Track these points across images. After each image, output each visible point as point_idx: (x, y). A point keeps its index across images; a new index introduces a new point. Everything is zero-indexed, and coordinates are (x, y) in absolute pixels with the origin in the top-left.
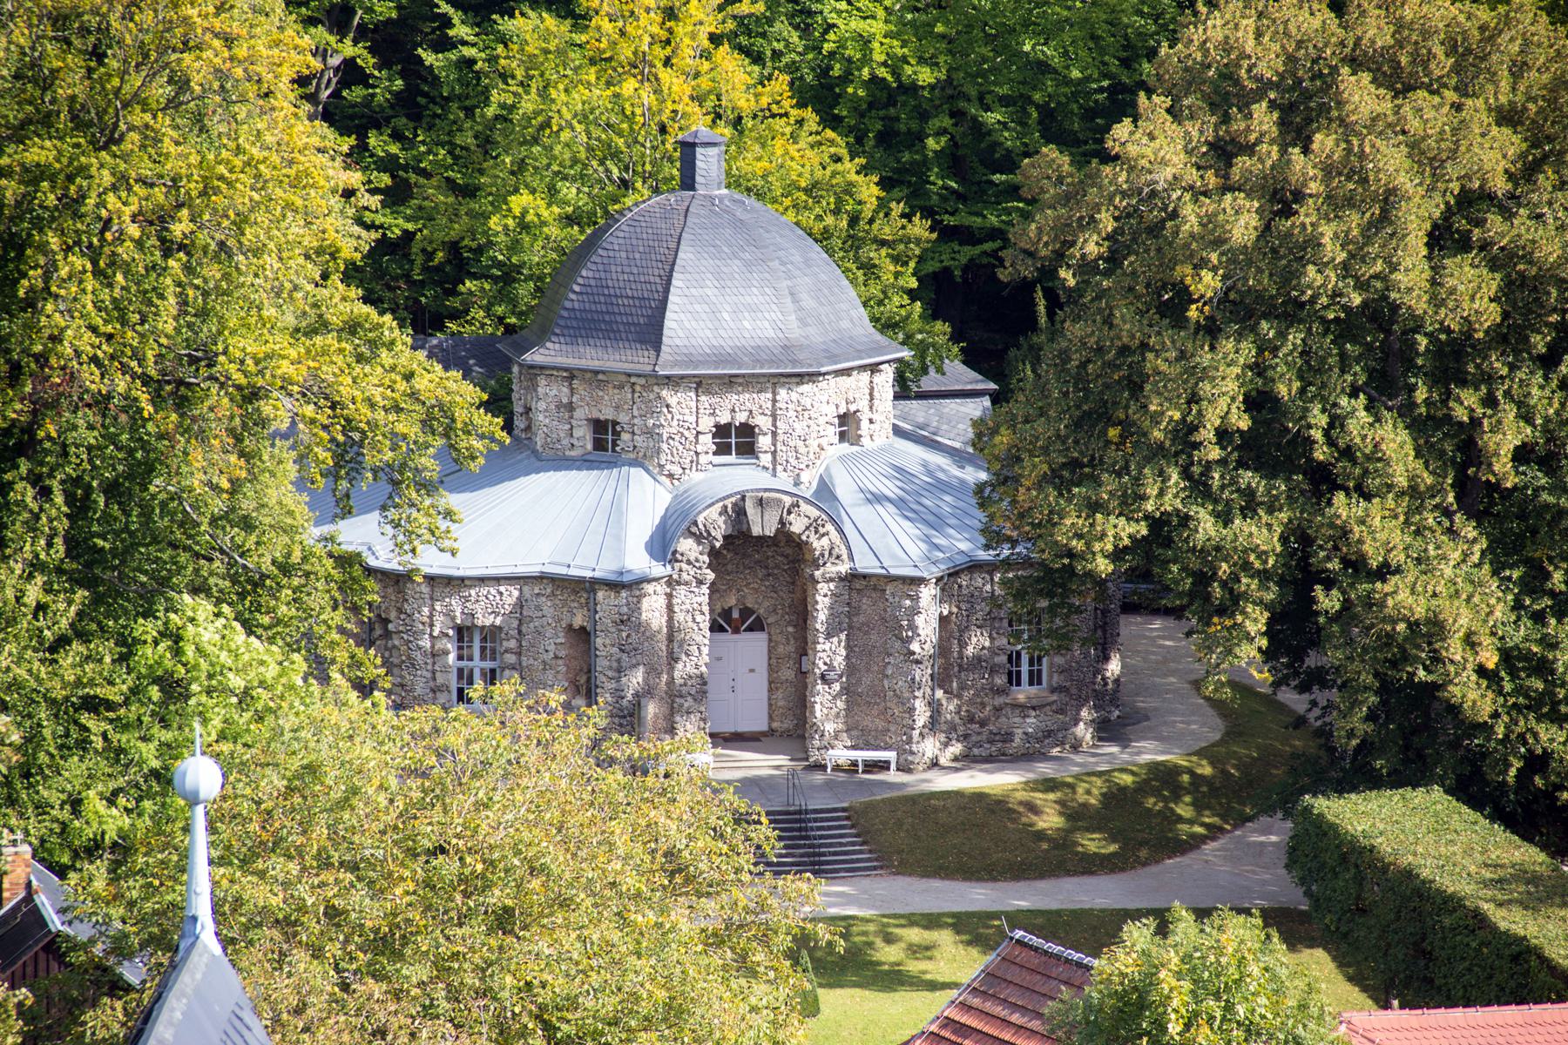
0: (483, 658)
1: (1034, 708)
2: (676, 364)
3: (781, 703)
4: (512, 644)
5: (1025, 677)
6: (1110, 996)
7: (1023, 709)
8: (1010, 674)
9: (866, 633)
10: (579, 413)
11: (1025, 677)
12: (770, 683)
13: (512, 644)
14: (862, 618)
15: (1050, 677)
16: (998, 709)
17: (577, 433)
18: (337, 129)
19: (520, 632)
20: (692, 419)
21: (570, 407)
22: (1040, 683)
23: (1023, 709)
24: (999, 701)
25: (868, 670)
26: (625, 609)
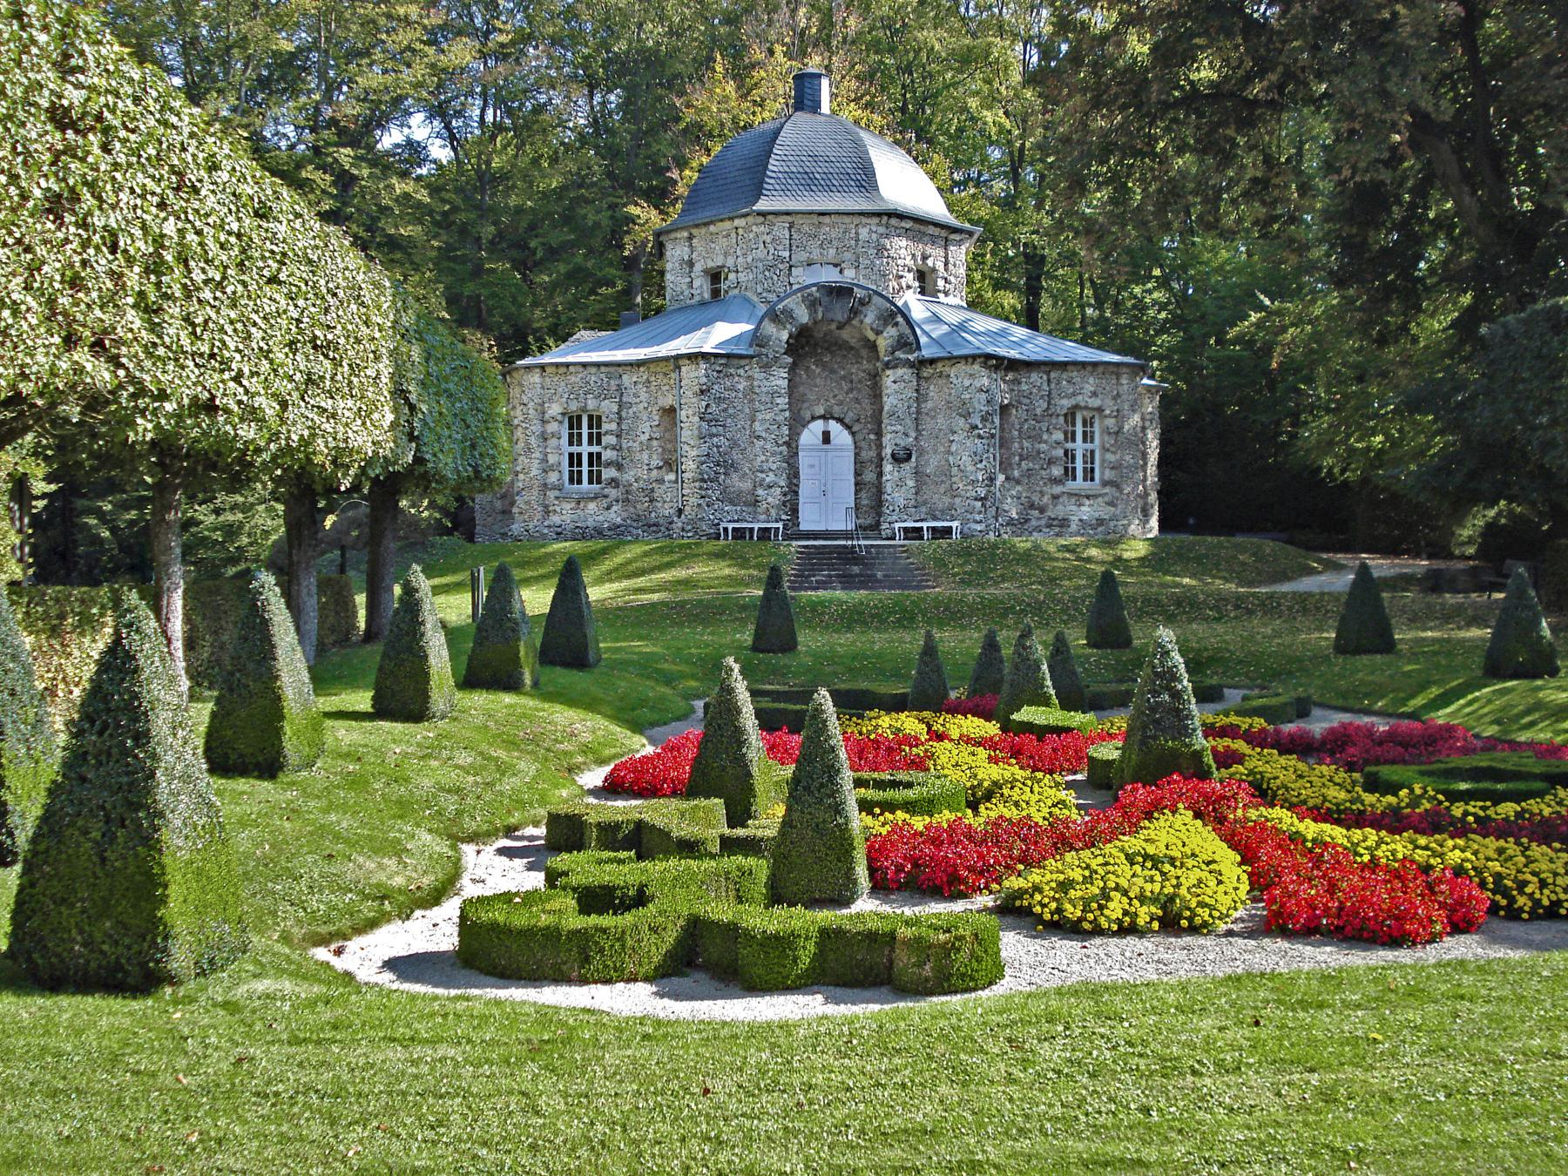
0: (590, 443)
1: (1088, 497)
2: (809, 182)
3: (865, 502)
4: (614, 426)
5: (1079, 473)
6: (638, 52)
7: (1078, 497)
8: (1066, 469)
9: (933, 418)
10: (698, 267)
11: (1079, 473)
12: (856, 484)
13: (614, 426)
14: (930, 405)
15: (1102, 473)
16: (1055, 497)
17: (696, 283)
18: (481, 926)
19: (620, 418)
20: (787, 254)
21: (691, 264)
22: (1092, 479)
23: (1078, 497)
24: (1057, 490)
25: (935, 452)
26: (704, 380)
